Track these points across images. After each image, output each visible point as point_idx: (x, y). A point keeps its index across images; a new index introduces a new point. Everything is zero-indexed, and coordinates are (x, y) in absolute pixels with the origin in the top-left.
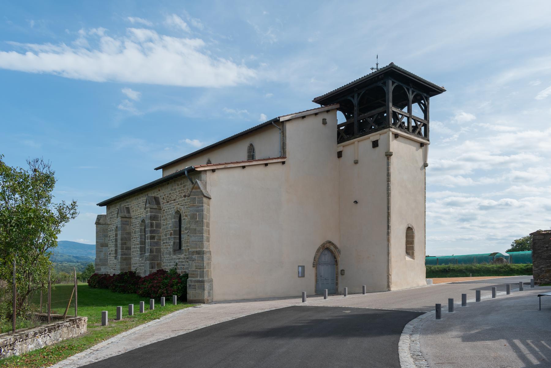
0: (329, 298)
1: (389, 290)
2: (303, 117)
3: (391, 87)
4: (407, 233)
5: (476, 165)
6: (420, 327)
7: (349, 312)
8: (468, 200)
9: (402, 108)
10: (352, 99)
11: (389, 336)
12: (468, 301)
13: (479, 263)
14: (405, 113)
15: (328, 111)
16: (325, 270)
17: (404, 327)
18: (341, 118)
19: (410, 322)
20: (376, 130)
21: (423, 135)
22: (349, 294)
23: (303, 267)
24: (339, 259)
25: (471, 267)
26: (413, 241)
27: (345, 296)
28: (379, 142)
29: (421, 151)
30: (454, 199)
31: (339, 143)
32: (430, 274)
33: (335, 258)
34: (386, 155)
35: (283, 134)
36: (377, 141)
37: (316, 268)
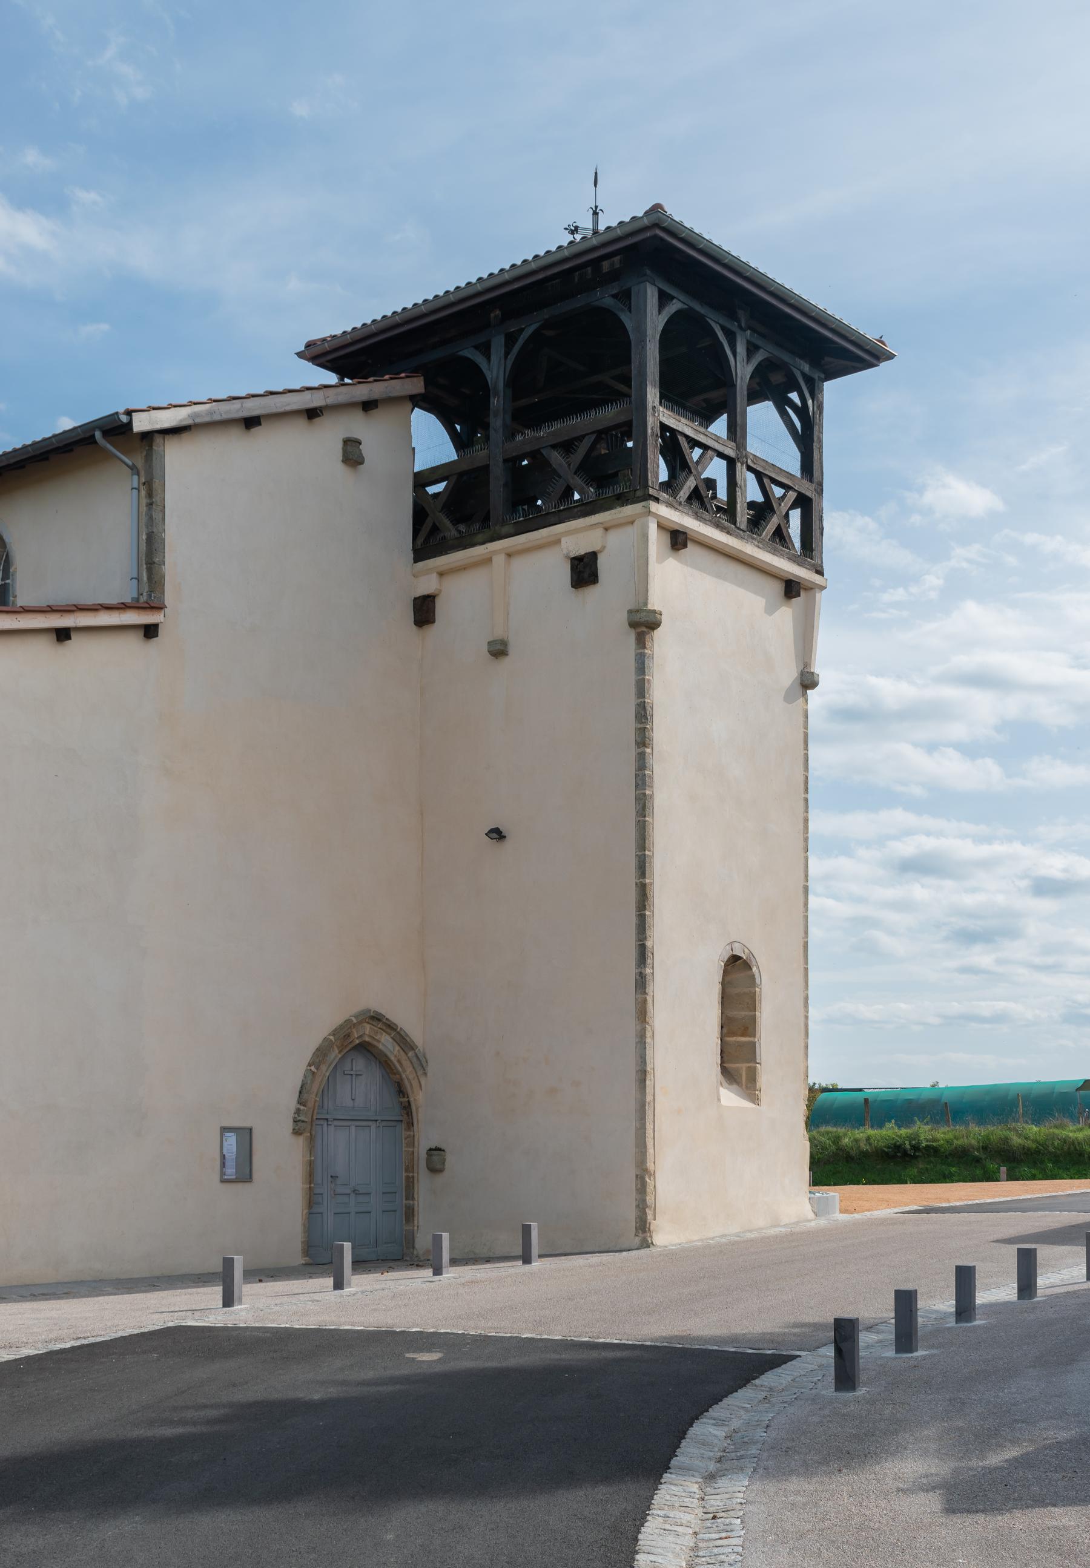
0: (360, 1284)
1: (646, 1244)
2: (251, 423)
3: (651, 317)
4: (725, 984)
5: (1012, 706)
6: (760, 1434)
7: (434, 1356)
8: (985, 851)
9: (707, 417)
10: (479, 359)
11: (602, 1491)
12: (982, 1298)
13: (1037, 1122)
14: (717, 439)
15: (368, 406)
16: (353, 1151)
17: (682, 1435)
18: (430, 441)
19: (716, 1411)
20: (588, 509)
21: (797, 544)
22: (454, 1262)
23: (246, 1135)
24: (419, 1098)
25: (1006, 1140)
26: (753, 1019)
27: (438, 1272)
28: (602, 562)
29: (787, 614)
30: (929, 844)
31: (420, 554)
32: (831, 1166)
33: (400, 1090)
34: (633, 625)
35: (150, 495)
36: (593, 555)
37: (311, 1140)
